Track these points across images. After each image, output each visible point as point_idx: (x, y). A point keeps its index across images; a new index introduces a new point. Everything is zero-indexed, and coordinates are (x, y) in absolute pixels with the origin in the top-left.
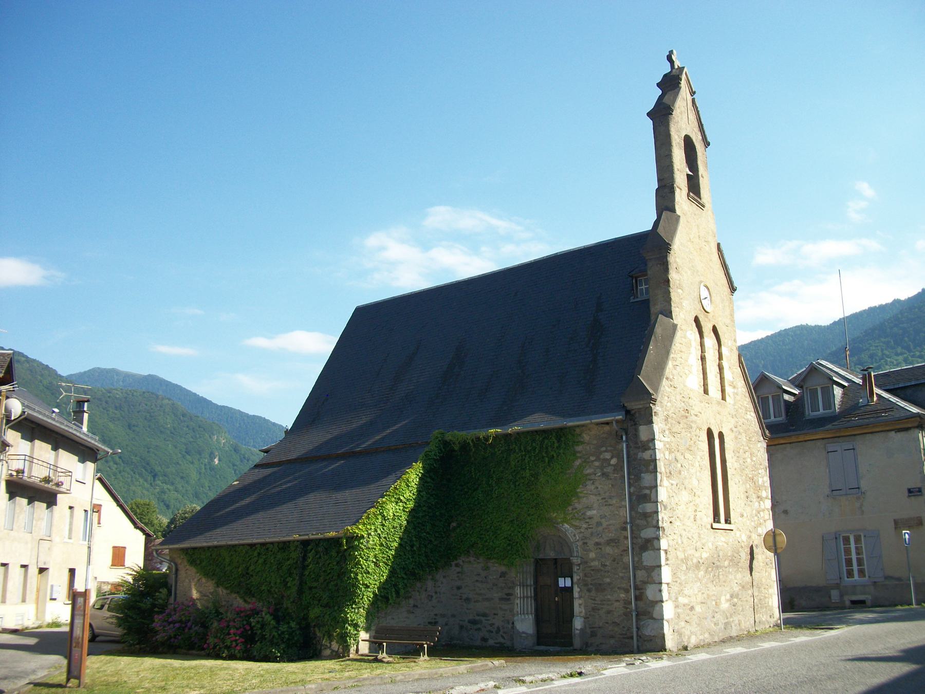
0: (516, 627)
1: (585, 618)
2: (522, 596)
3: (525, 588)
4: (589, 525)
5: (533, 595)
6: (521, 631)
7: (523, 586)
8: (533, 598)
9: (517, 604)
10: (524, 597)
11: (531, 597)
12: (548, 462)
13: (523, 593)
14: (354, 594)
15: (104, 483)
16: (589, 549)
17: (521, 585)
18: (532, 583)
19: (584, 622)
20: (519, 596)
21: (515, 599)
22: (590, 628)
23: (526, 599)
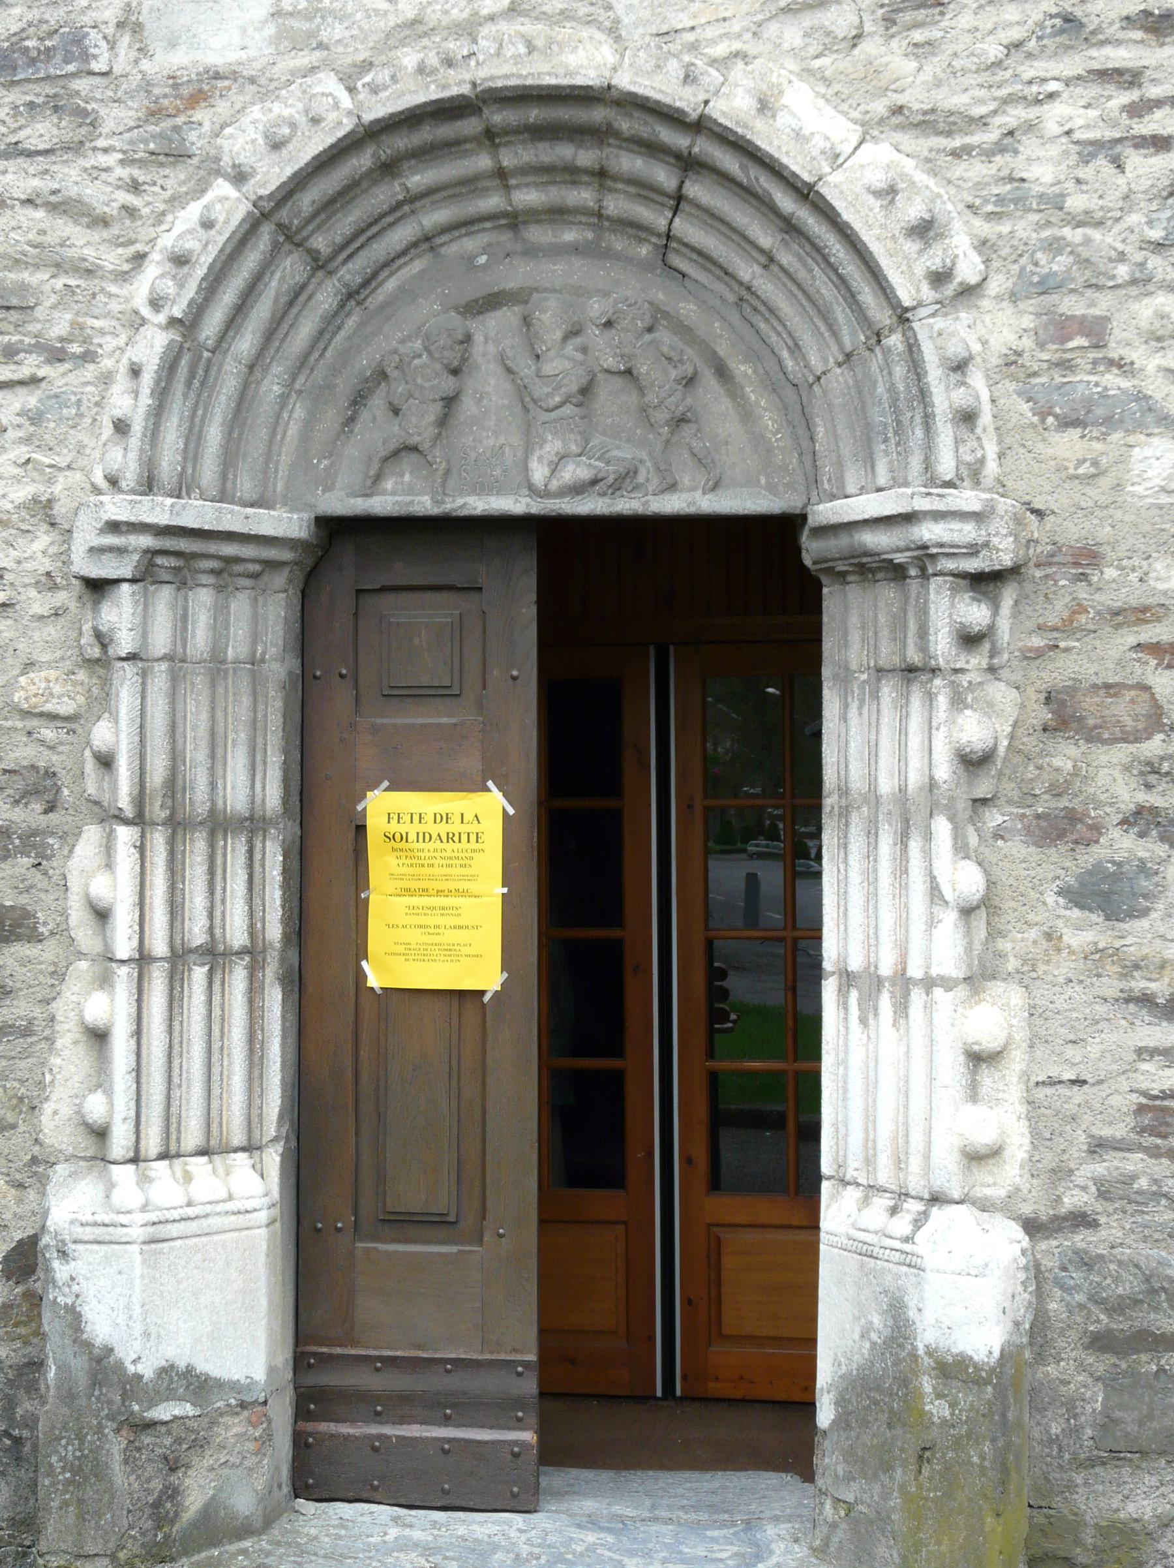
0: (74, 1318)
1: (1032, 1227)
2: (159, 946)
3: (197, 848)
4: (1136, 110)
5: (274, 931)
6: (146, 1370)
7: (177, 825)
8: (271, 971)
9: (99, 1037)
10: (179, 958)
11: (254, 952)
12: (49, 203)
13: (175, 909)
14: (1089, 873)
15: (251, 1051)
16: (1141, 397)
17: (157, 810)
18: (273, 796)
19: (1037, 1274)
20: (124, 947)
21: (59, 975)
22: (1100, 1342)
23: (199, 974)
